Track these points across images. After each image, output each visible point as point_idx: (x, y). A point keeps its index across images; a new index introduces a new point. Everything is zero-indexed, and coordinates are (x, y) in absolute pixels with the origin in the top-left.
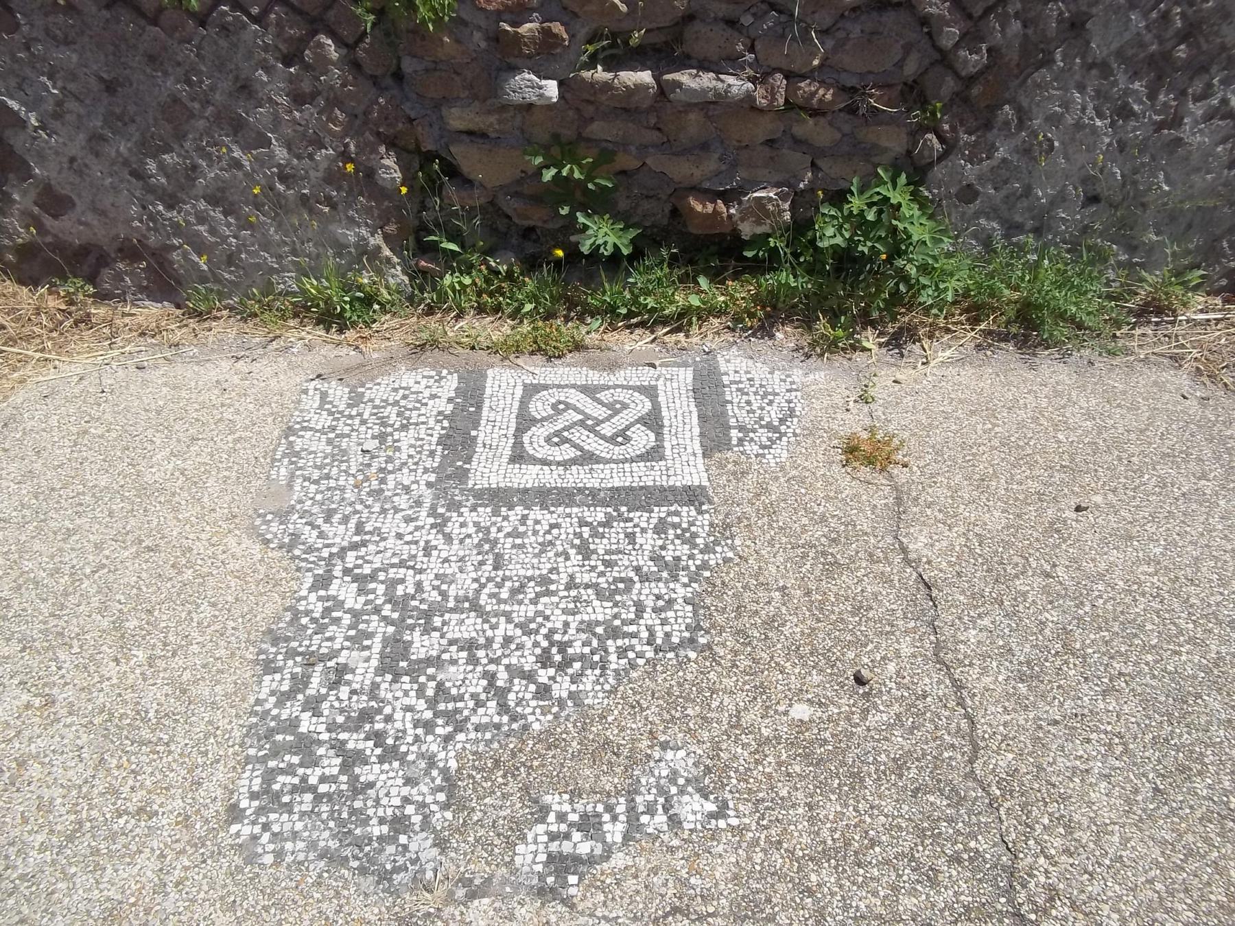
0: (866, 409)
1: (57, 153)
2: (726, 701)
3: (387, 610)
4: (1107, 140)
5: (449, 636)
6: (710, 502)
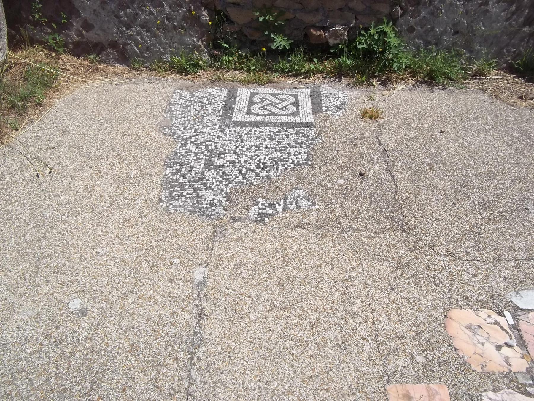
0: (371, 103)
1: (90, 8)
2: (317, 178)
3: (206, 153)
4: (462, 10)
5: (227, 160)
6: (315, 127)
